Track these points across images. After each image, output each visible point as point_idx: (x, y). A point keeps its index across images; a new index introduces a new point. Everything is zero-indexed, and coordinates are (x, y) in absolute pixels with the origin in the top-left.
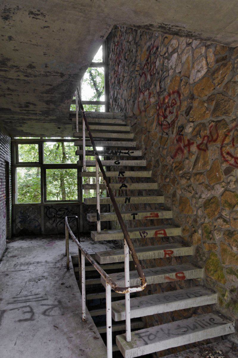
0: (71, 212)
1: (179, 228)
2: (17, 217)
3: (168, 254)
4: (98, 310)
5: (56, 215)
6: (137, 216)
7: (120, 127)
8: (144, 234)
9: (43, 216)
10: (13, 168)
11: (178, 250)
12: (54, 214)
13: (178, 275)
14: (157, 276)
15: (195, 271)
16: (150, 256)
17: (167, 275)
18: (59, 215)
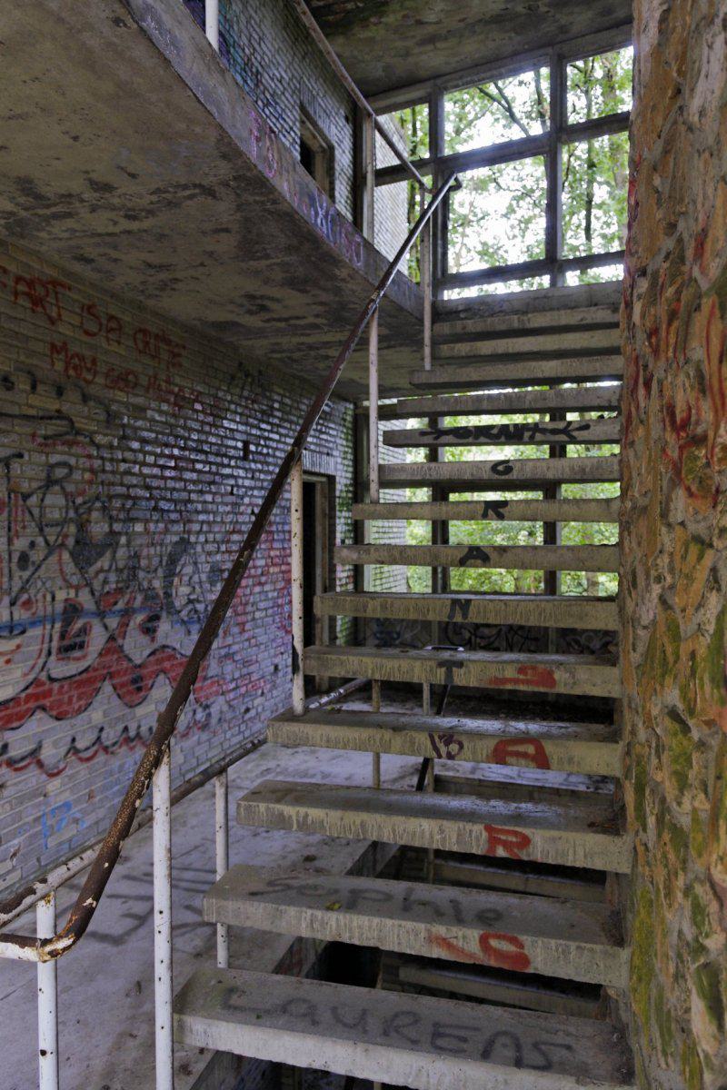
0: (520, 633)
1: (615, 746)
2: (368, 633)
3: (506, 844)
4: (466, 977)
5: (473, 638)
6: (462, 671)
7: (587, 335)
8: (447, 744)
9: (437, 635)
10: (359, 492)
11: (553, 840)
12: (467, 635)
13: (494, 943)
14: (397, 922)
15: (578, 947)
16: (422, 837)
17: (441, 930)
18: (482, 637)
